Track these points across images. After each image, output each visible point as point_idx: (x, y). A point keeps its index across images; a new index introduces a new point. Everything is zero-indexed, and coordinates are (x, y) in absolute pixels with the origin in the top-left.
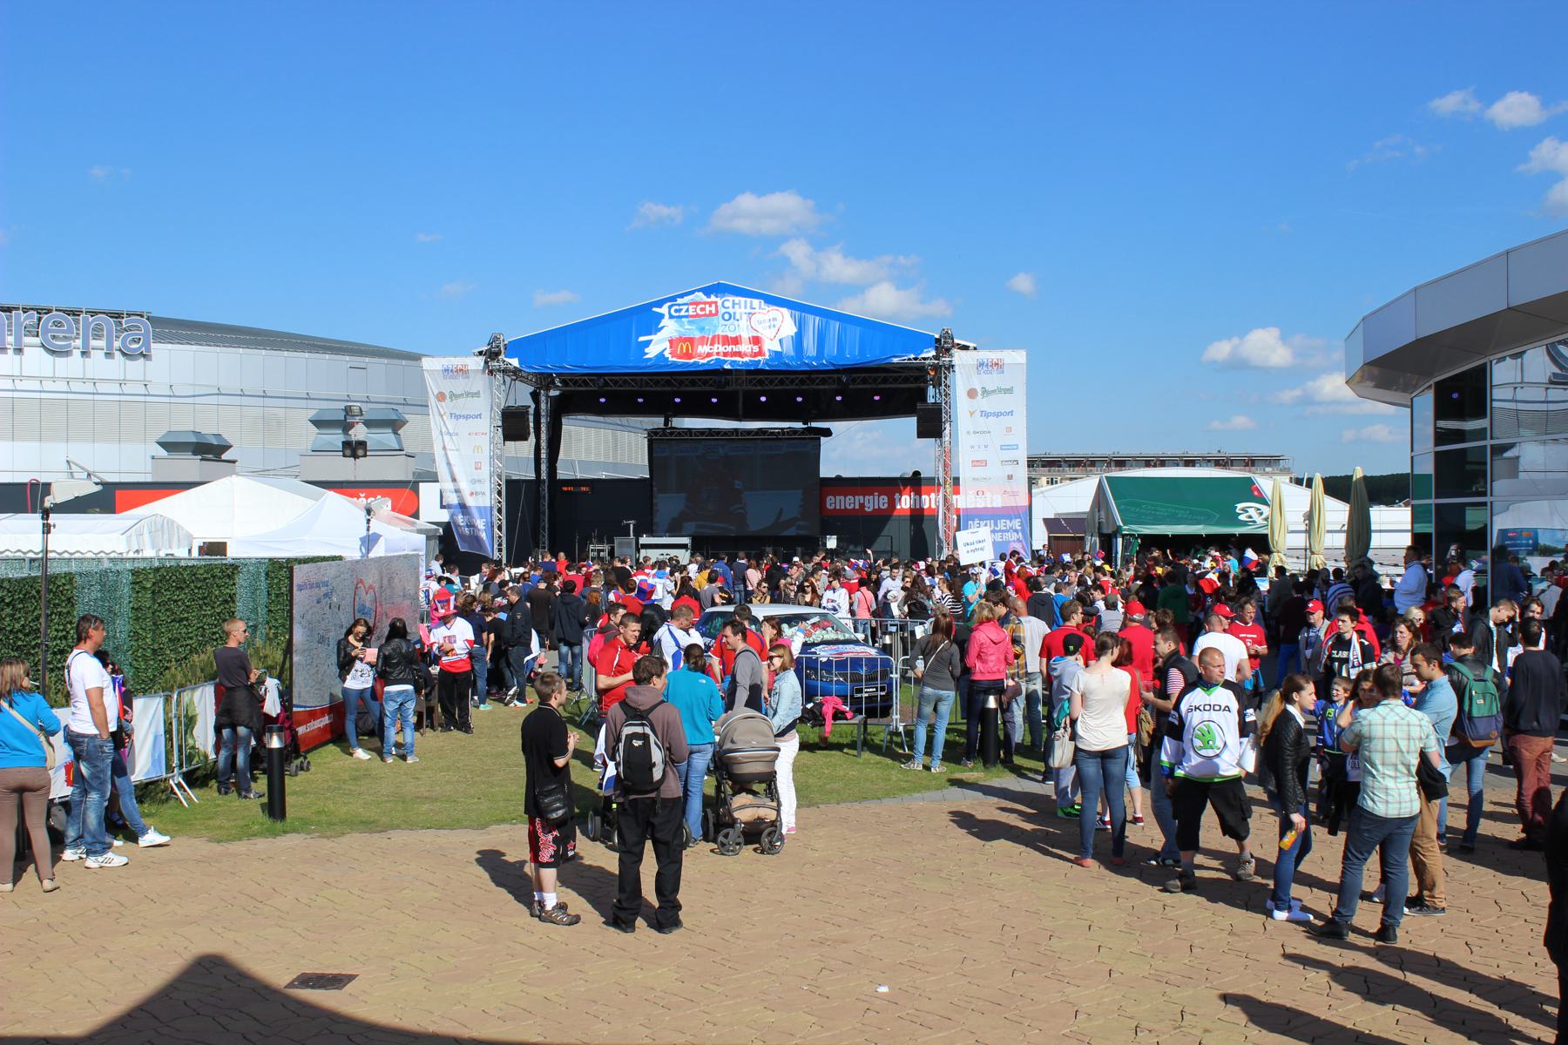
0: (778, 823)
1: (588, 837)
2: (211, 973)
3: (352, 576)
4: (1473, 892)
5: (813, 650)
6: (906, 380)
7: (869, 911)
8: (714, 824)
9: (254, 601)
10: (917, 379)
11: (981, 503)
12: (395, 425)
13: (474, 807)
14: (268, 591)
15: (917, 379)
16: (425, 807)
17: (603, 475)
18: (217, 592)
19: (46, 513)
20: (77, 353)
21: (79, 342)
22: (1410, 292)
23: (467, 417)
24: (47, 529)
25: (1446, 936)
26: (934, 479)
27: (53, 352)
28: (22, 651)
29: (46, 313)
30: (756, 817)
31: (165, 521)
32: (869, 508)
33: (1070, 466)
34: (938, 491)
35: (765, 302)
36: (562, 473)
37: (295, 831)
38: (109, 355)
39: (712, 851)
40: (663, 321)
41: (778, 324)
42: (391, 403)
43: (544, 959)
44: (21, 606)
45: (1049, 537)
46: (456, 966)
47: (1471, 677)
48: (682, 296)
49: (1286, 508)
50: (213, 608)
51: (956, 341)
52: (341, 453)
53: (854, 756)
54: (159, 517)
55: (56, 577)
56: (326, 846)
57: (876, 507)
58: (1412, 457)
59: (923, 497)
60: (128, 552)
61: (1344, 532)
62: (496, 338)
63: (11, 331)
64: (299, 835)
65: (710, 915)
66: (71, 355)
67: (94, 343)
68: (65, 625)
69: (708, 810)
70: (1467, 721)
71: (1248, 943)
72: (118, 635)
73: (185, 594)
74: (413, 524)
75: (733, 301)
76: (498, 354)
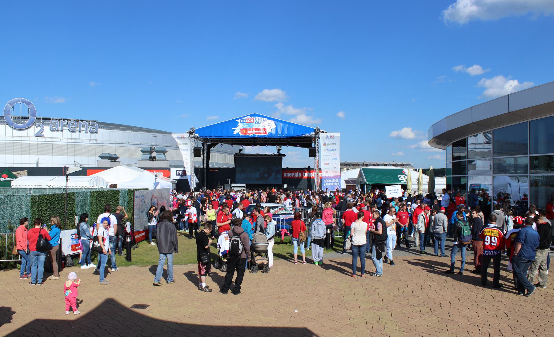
1: (215, 267)
5: (279, 216)
6: (306, 141)
9: (124, 201)
10: (309, 141)
12: (164, 152)
15: (309, 141)
17: (222, 167)
18: (114, 198)
19: (67, 176)
20: (78, 132)
21: (78, 129)
22: (445, 118)
24: (67, 180)
26: (314, 168)
27: (71, 132)
32: (296, 176)
33: (352, 165)
37: (133, 265)
39: (250, 272)
41: (270, 125)
43: (202, 301)
44: (60, 201)
45: (346, 185)
48: (244, 117)
49: (412, 178)
51: (320, 130)
55: (70, 193)
58: (446, 164)
59: (311, 173)
62: (192, 128)
67: (82, 129)
68: (72, 207)
74: (169, 179)
76: (193, 133)
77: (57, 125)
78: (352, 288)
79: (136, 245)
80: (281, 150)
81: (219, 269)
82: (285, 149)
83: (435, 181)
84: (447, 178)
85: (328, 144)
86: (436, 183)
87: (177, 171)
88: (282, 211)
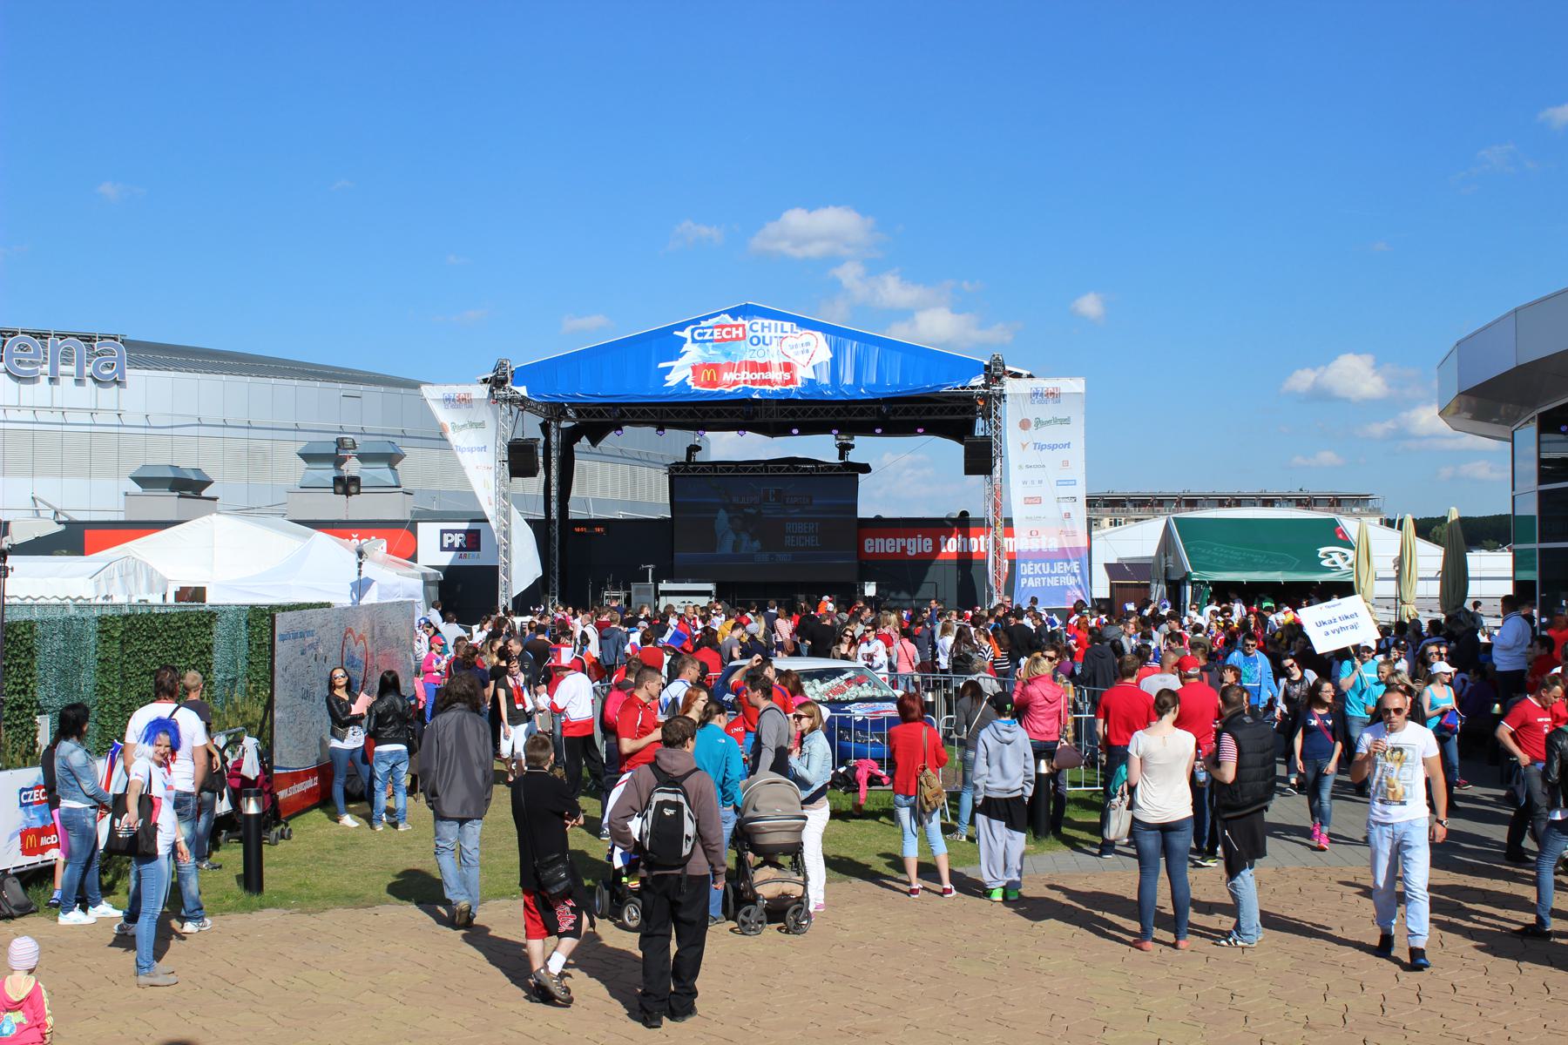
5: (847, 708)
6: (953, 411)
9: (234, 652)
10: (964, 410)
14: (249, 642)
15: (964, 410)
17: (620, 515)
18: (192, 643)
20: (44, 380)
21: (46, 368)
22: (1509, 314)
25: (1549, 1033)
26: (983, 519)
27: (18, 379)
29: (11, 336)
30: (780, 892)
32: (912, 552)
33: (1135, 506)
34: (988, 533)
35: (797, 325)
36: (575, 512)
37: (272, 905)
38: (79, 382)
39: (732, 930)
41: (811, 349)
45: (1111, 585)
48: (706, 318)
49: (1373, 553)
50: (187, 659)
52: (332, 490)
55: (15, 625)
56: (305, 922)
57: (920, 551)
58: (1513, 497)
59: (972, 539)
61: (1023, 576)
62: (502, 365)
66: (38, 381)
67: (62, 369)
68: (24, 678)
71: (1325, 1038)
72: (83, 689)
73: (156, 644)
74: (412, 567)
75: (763, 324)
76: (504, 381)
78: (1138, 992)
79: (283, 826)
80: (853, 446)
81: (611, 920)
85: (1039, 423)
87: (443, 532)
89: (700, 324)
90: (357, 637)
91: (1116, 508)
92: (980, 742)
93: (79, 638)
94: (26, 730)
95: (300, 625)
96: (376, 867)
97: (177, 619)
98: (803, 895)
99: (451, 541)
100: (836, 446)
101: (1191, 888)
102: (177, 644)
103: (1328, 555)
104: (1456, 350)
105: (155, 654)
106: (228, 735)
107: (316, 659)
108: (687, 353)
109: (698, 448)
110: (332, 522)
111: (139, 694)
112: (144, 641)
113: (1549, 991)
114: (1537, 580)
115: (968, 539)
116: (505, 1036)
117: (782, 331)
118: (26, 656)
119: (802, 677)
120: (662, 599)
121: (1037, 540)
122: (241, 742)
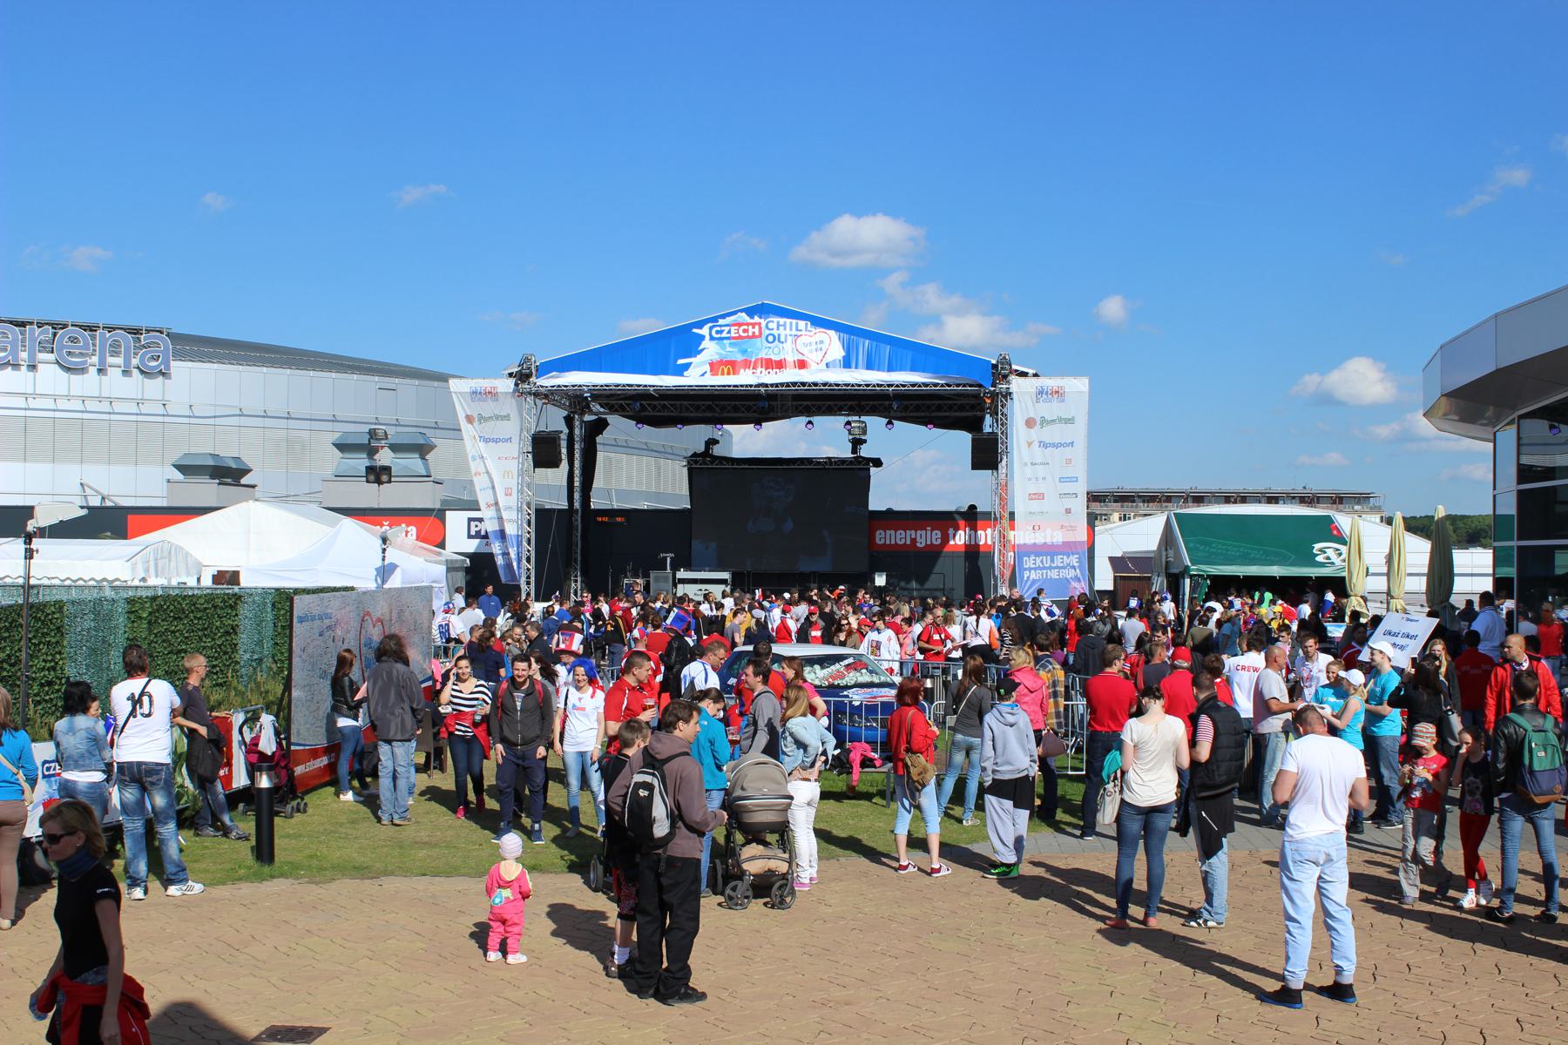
0: (790, 876)
1: (590, 887)
2: (176, 1023)
3: (358, 607)
4: (1531, 964)
5: (845, 693)
6: (962, 408)
7: (878, 971)
8: (722, 876)
9: (260, 633)
10: (973, 407)
11: (1039, 538)
12: (423, 450)
13: (474, 854)
14: (274, 623)
15: (973, 407)
16: (422, 853)
17: (645, 505)
18: (218, 624)
19: (29, 538)
20: (93, 371)
21: (95, 359)
22: (1491, 318)
23: (496, 441)
24: (29, 554)
25: (1496, 1012)
26: (990, 513)
27: (68, 370)
28: (7, 682)
29: (63, 328)
30: (766, 869)
31: (173, 549)
32: (921, 544)
33: (1144, 502)
34: (995, 527)
35: (811, 324)
36: (596, 502)
37: (282, 875)
38: (126, 373)
39: (720, 904)
40: (703, 343)
41: (824, 347)
42: (419, 427)
43: (528, 1016)
44: (6, 635)
45: (1115, 577)
46: (434, 1022)
47: (1529, 728)
48: (723, 317)
49: (1364, 549)
50: (213, 639)
51: (1014, 367)
52: (364, 479)
53: (883, 806)
54: (166, 543)
55: (45, 605)
56: (312, 892)
57: (929, 543)
58: (1494, 496)
59: (979, 532)
60: (132, 581)
61: (1026, 569)
62: (527, 360)
63: (25, 346)
64: (286, 880)
65: (708, 972)
66: (87, 372)
67: (111, 360)
68: (53, 655)
69: (718, 861)
70: (1528, 776)
71: (1280, 1014)
72: (112, 667)
73: (183, 624)
74: (439, 554)
75: (778, 322)
76: (529, 376)
77: (14, 343)
78: (1104, 968)
79: (299, 800)
80: (865, 441)
81: (604, 893)
82: (881, 436)
83: (1455, 562)
84: (1494, 549)
85: (1044, 422)
86: (1456, 571)
87: (470, 520)
88: (858, 674)
89: (718, 322)
90: (374, 619)
91: (1126, 504)
92: (986, 725)
93: (109, 617)
94: (56, 705)
95: (319, 608)
96: (385, 840)
97: (203, 601)
98: (788, 872)
99: (478, 529)
100: (849, 441)
101: (1166, 869)
102: (204, 624)
103: (1322, 551)
104: (1439, 355)
105: (182, 634)
106: (247, 712)
107: (333, 641)
108: (705, 351)
109: (715, 442)
110: (364, 510)
111: (166, 672)
112: (171, 622)
113: (1500, 972)
114: (1515, 576)
115: (976, 531)
116: (492, 1002)
117: (797, 330)
118: (55, 634)
119: (804, 662)
120: (680, 587)
121: (1042, 534)
122: (258, 719)
